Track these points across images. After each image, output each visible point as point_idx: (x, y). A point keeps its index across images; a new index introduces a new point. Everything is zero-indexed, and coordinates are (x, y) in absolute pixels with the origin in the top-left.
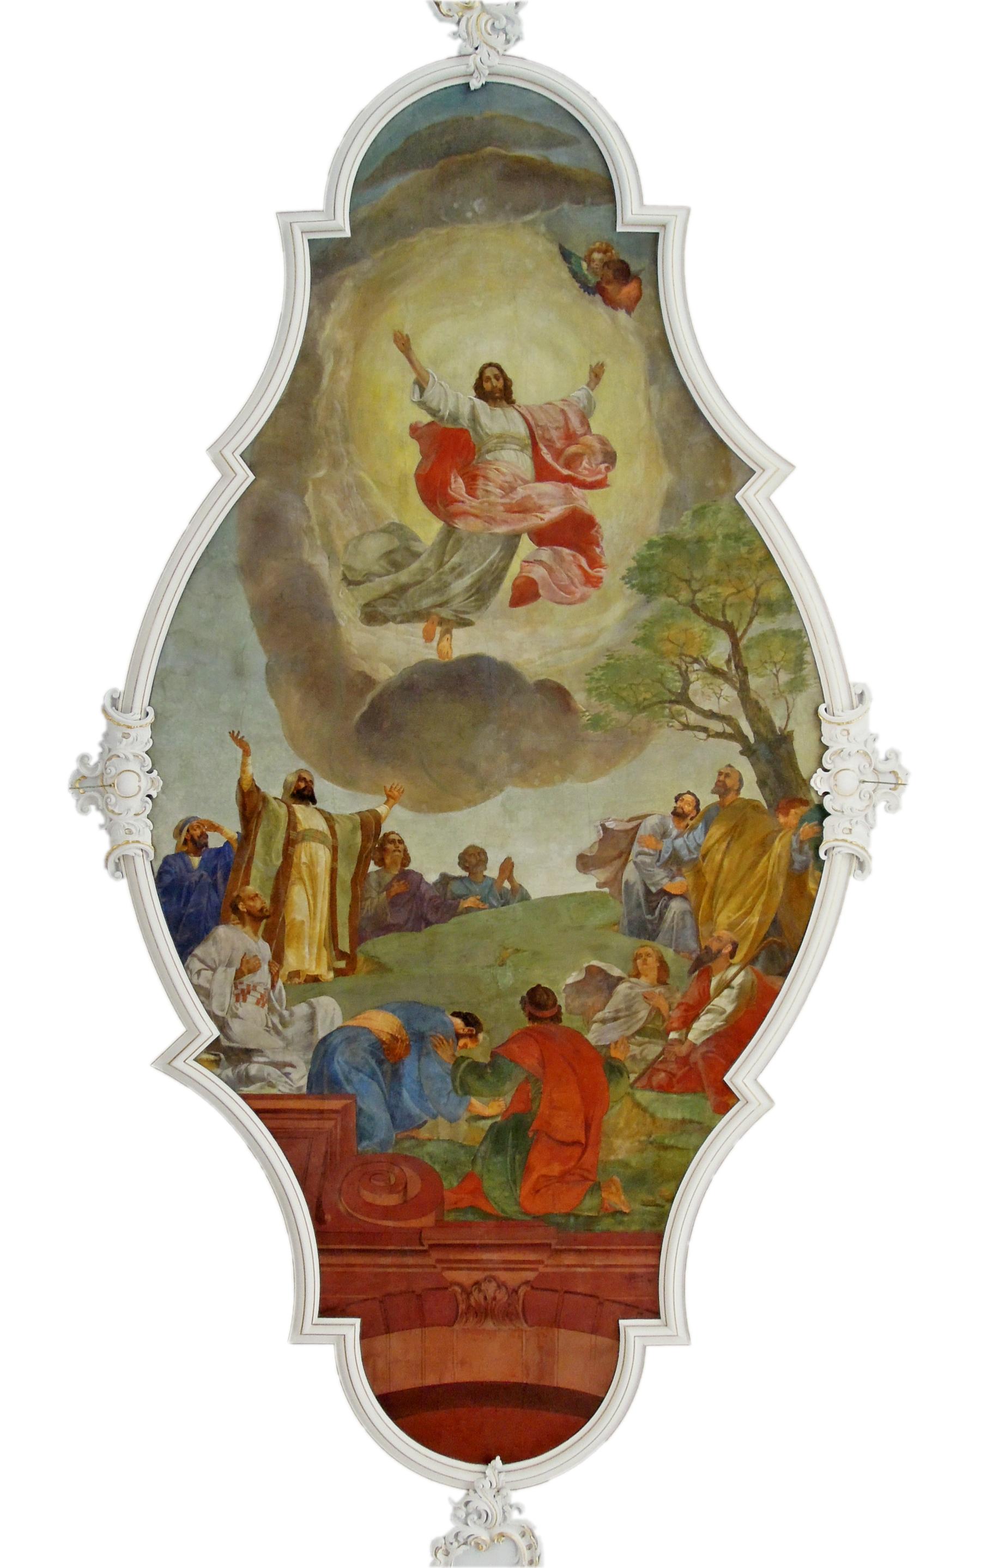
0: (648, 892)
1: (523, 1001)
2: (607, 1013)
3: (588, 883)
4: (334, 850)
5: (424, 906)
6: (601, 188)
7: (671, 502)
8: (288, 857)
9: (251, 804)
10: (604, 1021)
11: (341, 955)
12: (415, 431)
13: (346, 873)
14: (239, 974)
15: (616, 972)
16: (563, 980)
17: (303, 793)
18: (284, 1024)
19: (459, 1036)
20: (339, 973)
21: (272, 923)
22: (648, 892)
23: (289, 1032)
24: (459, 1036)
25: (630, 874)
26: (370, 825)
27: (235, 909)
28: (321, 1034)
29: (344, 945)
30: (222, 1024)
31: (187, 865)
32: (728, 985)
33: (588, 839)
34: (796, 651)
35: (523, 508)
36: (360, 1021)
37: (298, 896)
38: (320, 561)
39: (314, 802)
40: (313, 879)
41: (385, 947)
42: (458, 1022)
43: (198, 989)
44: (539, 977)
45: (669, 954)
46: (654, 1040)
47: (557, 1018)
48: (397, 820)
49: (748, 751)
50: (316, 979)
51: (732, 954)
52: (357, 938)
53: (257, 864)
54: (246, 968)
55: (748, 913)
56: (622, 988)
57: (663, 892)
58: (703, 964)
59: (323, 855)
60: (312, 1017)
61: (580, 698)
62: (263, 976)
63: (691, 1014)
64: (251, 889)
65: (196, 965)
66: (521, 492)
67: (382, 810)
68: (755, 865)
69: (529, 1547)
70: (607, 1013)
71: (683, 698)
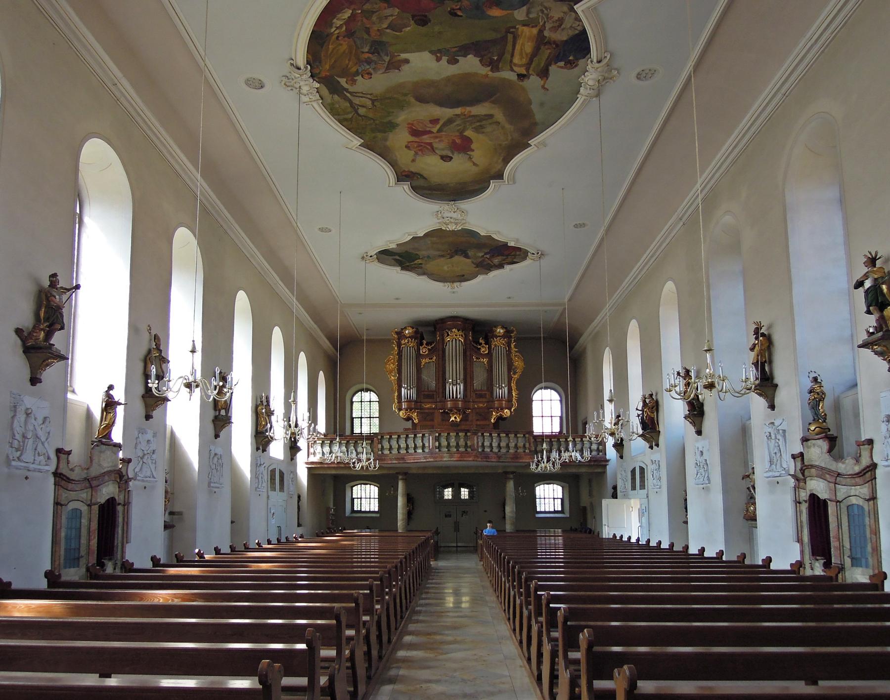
0: (379, 54)
1: (430, 21)
2: (391, 18)
3: (404, 56)
4: (511, 61)
5: (476, 48)
6: (414, 188)
7: (386, 140)
8: (531, 61)
9: (544, 73)
10: (392, 15)
11: (512, 33)
12: (473, 150)
13: (507, 56)
14: (560, 26)
15: (388, 31)
16: (411, 28)
17: (521, 77)
18: (542, 11)
19: (459, 9)
20: (514, 27)
21: (541, 41)
22: (379, 54)
23: (540, 8)
24: (459, 9)
25: (387, 59)
26: (494, 66)
27: (557, 46)
28: (525, 8)
29: (510, 36)
30: (572, 9)
31: (575, 56)
32: (337, 28)
33: (405, 68)
34: (333, 111)
35: (436, 137)
36: (505, 13)
37: (529, 48)
38: (507, 126)
39: (518, 75)
40: (521, 54)
41: (490, 36)
42: (459, 13)
43: (580, 20)
44: (423, 30)
45: (366, 36)
46: (420, 472)
47: (413, 17)
48: (485, 71)
49: (347, 90)
50: (524, 25)
51: (338, 37)
52: (504, 39)
53: (544, 59)
54: (555, 29)
55: (334, 49)
56: (385, 26)
57: (373, 53)
58: (350, 34)
59: (516, 60)
60: (528, 13)
61: (413, 100)
62: (548, 26)
63: (353, 17)
64: (549, 51)
65: (579, 28)
66: (437, 140)
67: (490, 73)
68: (335, 61)
69: (422, 100)
70: (391, 18)
71: (373, 101)
